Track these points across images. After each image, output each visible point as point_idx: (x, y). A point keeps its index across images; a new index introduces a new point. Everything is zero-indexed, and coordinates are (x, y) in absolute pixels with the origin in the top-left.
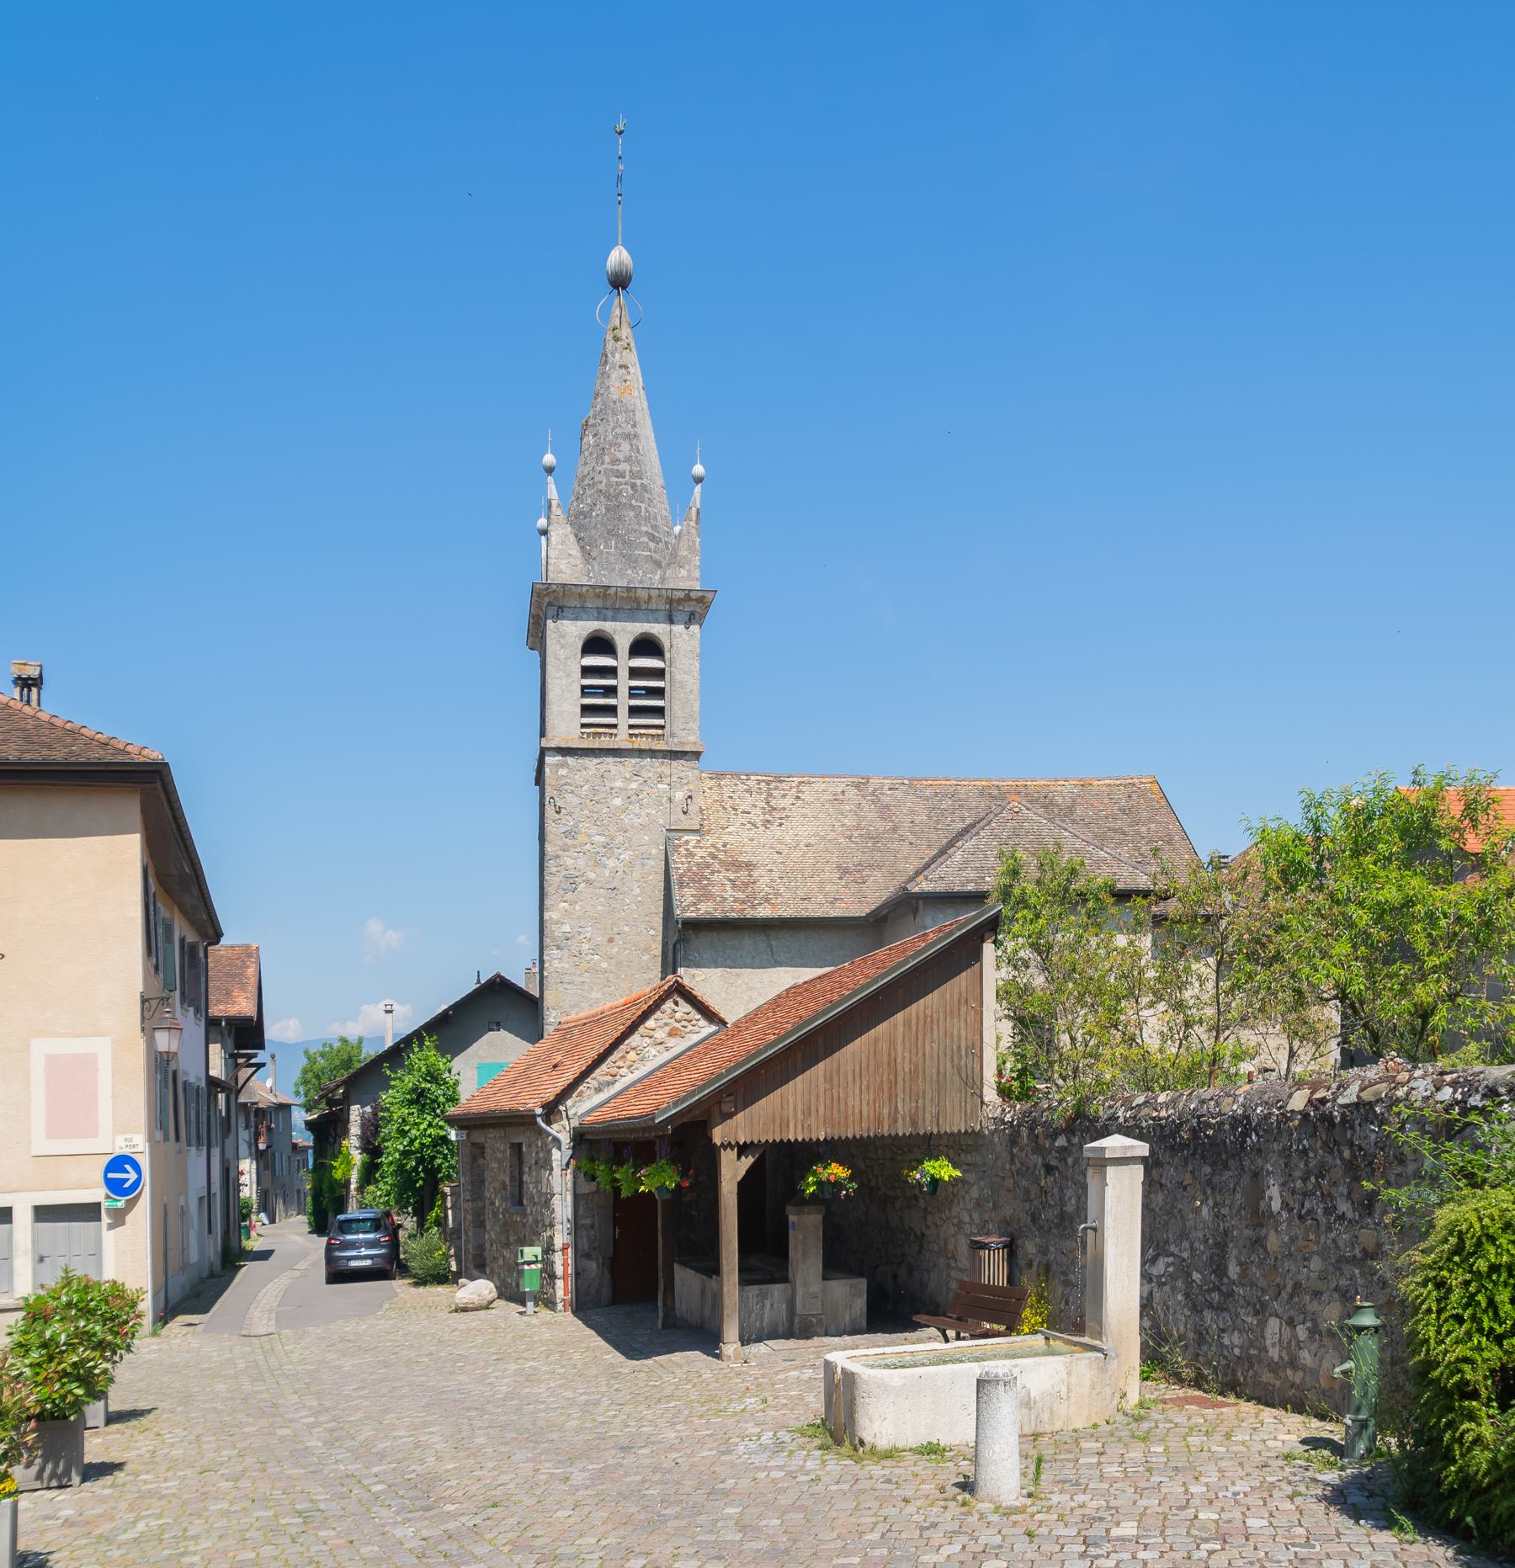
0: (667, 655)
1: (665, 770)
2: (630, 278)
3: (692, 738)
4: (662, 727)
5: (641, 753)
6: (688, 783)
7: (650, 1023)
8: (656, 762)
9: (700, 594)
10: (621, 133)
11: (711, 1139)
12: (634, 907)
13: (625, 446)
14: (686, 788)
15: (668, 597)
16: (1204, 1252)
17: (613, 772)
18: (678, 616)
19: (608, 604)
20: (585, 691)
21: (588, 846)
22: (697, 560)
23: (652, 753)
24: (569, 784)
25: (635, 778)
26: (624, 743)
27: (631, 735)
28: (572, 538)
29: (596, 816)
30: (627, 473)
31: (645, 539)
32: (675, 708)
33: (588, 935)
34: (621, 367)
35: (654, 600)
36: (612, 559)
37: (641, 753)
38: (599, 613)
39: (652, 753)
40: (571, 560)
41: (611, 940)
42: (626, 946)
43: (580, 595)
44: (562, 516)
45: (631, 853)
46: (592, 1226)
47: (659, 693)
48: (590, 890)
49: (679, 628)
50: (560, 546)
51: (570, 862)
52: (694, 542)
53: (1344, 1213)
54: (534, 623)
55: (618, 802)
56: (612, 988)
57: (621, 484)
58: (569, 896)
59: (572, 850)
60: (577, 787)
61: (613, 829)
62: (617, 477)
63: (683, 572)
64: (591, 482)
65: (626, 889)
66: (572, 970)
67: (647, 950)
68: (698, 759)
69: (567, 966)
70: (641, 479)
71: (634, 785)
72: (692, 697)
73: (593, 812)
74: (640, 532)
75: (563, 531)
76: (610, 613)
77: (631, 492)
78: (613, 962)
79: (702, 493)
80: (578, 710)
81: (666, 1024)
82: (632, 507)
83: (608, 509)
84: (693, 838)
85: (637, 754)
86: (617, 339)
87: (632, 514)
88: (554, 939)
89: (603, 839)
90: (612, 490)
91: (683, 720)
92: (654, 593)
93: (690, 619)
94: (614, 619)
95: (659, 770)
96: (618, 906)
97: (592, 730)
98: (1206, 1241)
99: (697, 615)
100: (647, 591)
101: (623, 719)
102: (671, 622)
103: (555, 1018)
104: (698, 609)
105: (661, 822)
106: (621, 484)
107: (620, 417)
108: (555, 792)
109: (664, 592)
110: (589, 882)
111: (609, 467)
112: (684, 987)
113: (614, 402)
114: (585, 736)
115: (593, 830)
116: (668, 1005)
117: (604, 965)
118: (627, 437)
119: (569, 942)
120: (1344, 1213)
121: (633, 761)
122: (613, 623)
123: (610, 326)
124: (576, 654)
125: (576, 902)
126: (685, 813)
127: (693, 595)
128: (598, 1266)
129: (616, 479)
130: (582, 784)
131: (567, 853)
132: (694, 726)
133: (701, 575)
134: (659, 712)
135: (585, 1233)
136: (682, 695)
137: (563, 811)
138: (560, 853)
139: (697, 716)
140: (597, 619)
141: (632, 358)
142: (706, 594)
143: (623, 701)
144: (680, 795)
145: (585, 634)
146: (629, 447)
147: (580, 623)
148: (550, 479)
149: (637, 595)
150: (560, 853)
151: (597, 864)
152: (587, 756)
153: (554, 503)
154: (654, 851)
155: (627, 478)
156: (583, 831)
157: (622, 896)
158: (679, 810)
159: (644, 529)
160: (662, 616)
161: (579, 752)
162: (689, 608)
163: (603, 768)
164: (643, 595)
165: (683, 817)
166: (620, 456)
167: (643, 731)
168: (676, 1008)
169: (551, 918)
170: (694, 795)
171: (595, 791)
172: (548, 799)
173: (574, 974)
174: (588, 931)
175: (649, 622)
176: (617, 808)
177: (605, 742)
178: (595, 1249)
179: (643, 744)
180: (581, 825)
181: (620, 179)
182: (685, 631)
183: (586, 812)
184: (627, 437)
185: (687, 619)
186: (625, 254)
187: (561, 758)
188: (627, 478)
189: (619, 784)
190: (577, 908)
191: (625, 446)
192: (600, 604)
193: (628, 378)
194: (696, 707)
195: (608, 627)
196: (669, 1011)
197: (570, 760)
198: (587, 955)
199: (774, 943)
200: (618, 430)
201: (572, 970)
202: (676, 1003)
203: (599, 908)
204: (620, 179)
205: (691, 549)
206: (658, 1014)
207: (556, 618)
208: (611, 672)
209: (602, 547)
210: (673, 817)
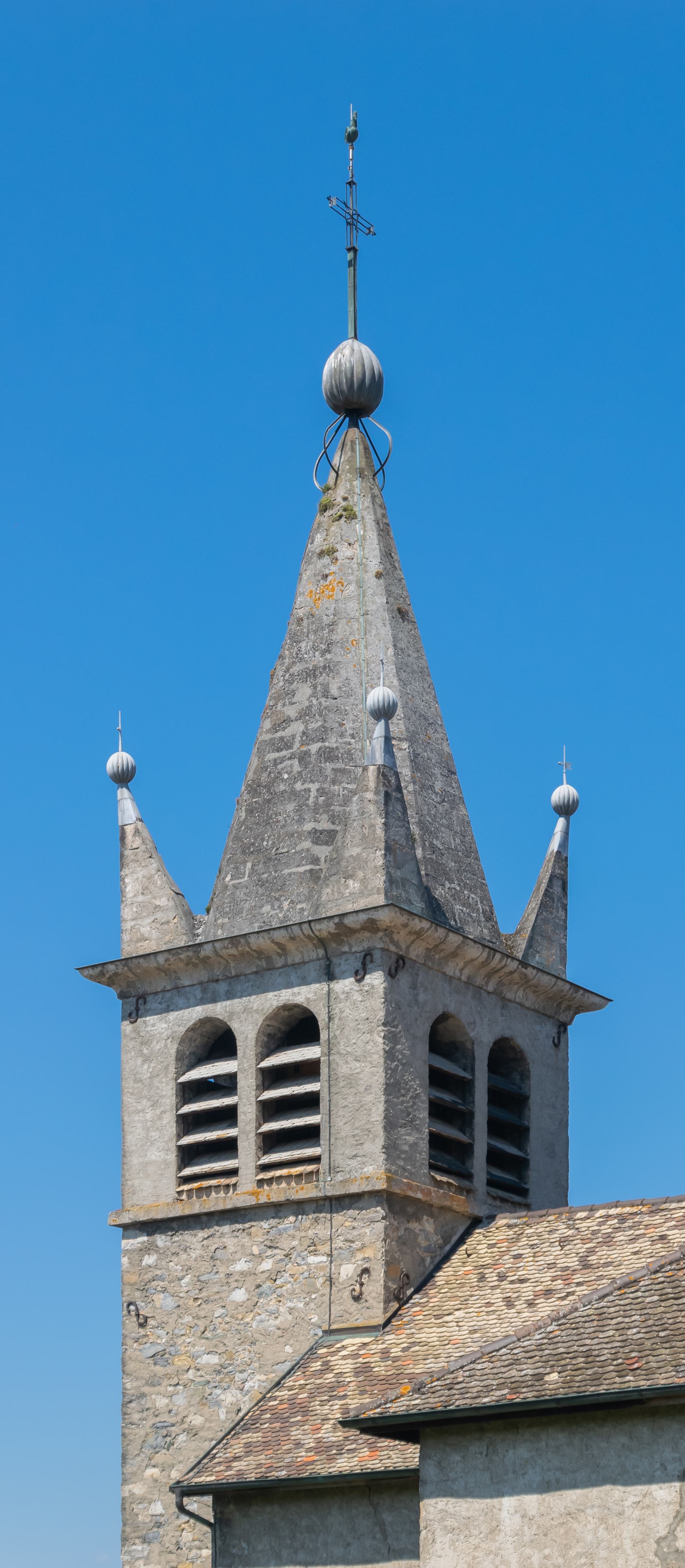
0: (323, 1036)
3: (369, 1170)
4: (316, 1160)
5: (277, 1209)
8: (306, 1220)
10: (352, 138)
14: (360, 1256)
17: (231, 1249)
18: (341, 964)
19: (218, 972)
21: (191, 1374)
23: (298, 1207)
27: (261, 1183)
29: (202, 1324)
31: (307, 844)
32: (338, 1123)
36: (240, 894)
37: (277, 1209)
38: (204, 991)
39: (298, 1207)
40: (159, 915)
47: (311, 1102)
48: (193, 1445)
49: (345, 985)
50: (140, 898)
51: (161, 1402)
55: (239, 1295)
58: (161, 1457)
59: (166, 1382)
61: (231, 1341)
63: (354, 885)
73: (198, 1317)
74: (300, 835)
76: (222, 987)
77: (297, 767)
89: (214, 1360)
90: (264, 777)
92: (280, 936)
93: (364, 964)
94: (230, 995)
97: (195, 1185)
102: (330, 976)
105: (315, 1318)
124: (167, 1068)
126: (357, 1299)
129: (276, 755)
134: (311, 1134)
137: (151, 1322)
138: (146, 1389)
140: (202, 1002)
144: (347, 1271)
147: (172, 1016)
148: (123, 794)
150: (146, 1389)
151: (204, 1401)
153: (129, 830)
158: (347, 1294)
159: (308, 826)
160: (312, 970)
162: (359, 944)
163: (214, 1243)
164: (262, 943)
165: (353, 1307)
166: (291, 712)
171: (201, 1284)
177: (216, 1202)
179: (276, 1193)
182: (356, 986)
183: (188, 1319)
184: (311, 674)
185: (358, 965)
189: (241, 1266)
191: (303, 692)
195: (219, 1010)
197: (161, 1240)
199: (387, 1517)
209: (228, 878)
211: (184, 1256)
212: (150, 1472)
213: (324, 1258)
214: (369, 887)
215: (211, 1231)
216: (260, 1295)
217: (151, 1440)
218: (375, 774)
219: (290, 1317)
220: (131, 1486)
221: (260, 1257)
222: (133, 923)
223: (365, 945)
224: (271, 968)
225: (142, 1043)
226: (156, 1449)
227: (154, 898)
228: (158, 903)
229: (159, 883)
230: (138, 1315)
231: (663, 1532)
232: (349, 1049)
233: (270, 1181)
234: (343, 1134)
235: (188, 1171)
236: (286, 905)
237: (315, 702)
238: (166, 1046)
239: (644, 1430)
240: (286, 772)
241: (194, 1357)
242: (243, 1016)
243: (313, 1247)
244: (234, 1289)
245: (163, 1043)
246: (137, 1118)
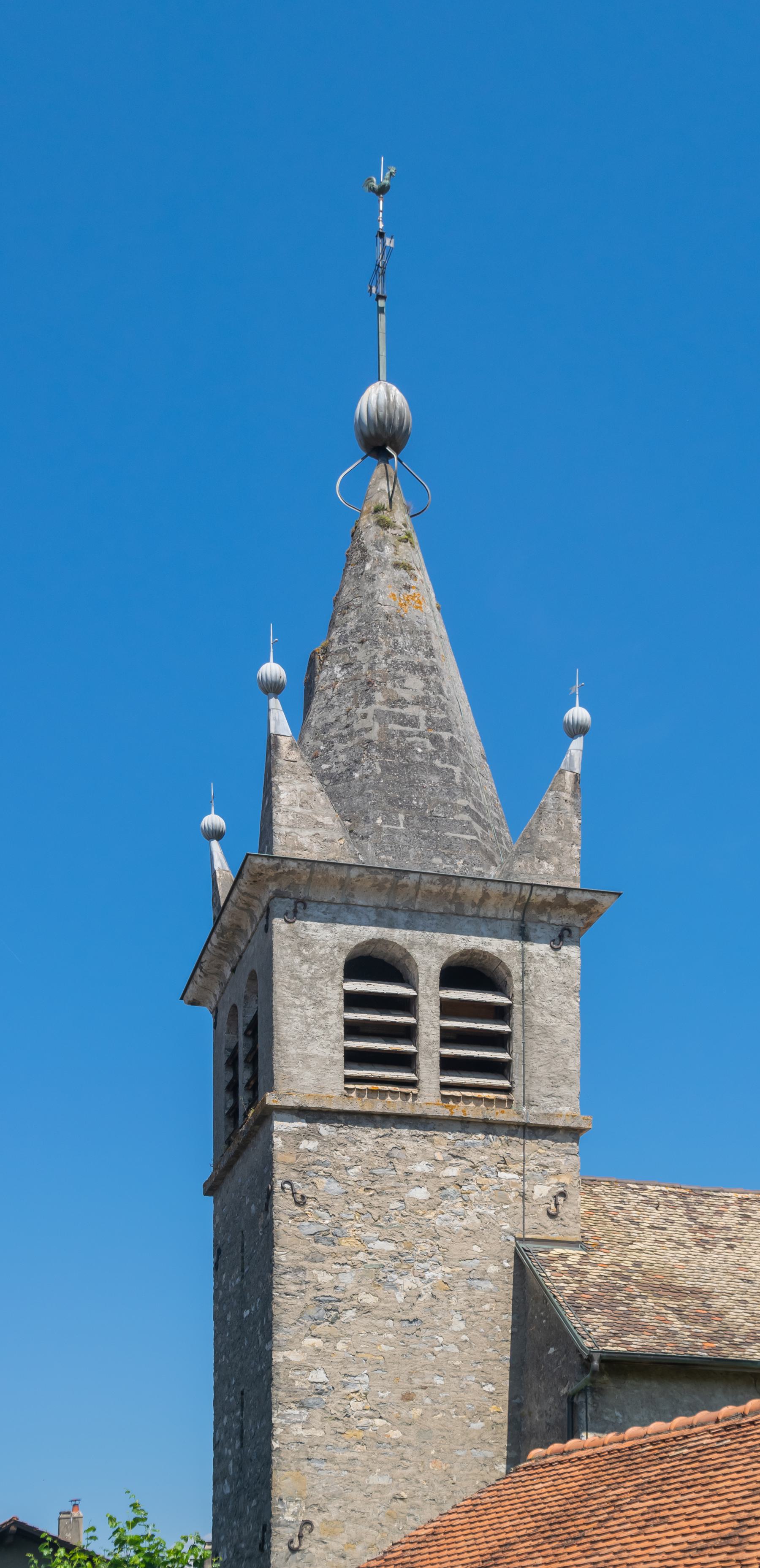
0: (517, 987)
1: (515, 1152)
2: (406, 435)
3: (565, 1109)
4: (507, 1091)
5: (465, 1124)
6: (559, 1173)
8: (496, 1141)
9: (588, 896)
12: (453, 1348)
13: (415, 683)
14: (554, 1180)
15: (520, 898)
17: (410, 1151)
19: (399, 902)
20: (501, 1041)
21: (362, 1256)
22: (575, 851)
24: (322, 1164)
25: (454, 1161)
26: (433, 1108)
28: (322, 799)
29: (375, 1213)
30: (422, 721)
33: (363, 1388)
34: (396, 565)
35: (491, 902)
38: (379, 915)
39: (489, 1127)
40: (321, 831)
41: (407, 1397)
42: (437, 1406)
43: (343, 884)
44: (302, 763)
45: (448, 1270)
47: (501, 1041)
48: (365, 1321)
50: (298, 809)
51: (324, 1278)
52: (568, 823)
54: (220, 946)
55: (421, 1194)
56: (412, 1470)
57: (410, 735)
58: (323, 1328)
59: (330, 1260)
60: (338, 1168)
62: (401, 724)
64: (345, 732)
65: (438, 1322)
66: (331, 1440)
67: (480, 1414)
68: (576, 1140)
69: (320, 1433)
70: (450, 730)
72: (566, 1050)
75: (304, 786)
76: (402, 917)
77: (430, 747)
78: (413, 1429)
79: (586, 752)
80: (340, 1056)
82: (433, 769)
83: (386, 768)
85: (459, 1126)
86: (385, 525)
87: (435, 779)
88: (292, 1392)
89: (391, 1247)
91: (549, 1082)
93: (561, 937)
95: (502, 1152)
96: (422, 1346)
99: (575, 932)
100: (482, 884)
102: (524, 935)
103: (294, 1514)
104: (578, 922)
105: (507, 1227)
106: (410, 735)
107: (400, 640)
108: (294, 1174)
109: (516, 889)
110: (363, 1310)
111: (385, 708)
113: (388, 617)
114: (354, 1094)
115: (371, 1233)
117: (396, 1434)
118: (418, 669)
119: (324, 1398)
121: (450, 1136)
122: (408, 932)
123: (370, 506)
124: (333, 974)
125: (338, 1338)
126: (552, 1216)
127: (572, 897)
130: (349, 1164)
131: (318, 1265)
132: (572, 1092)
133: (581, 873)
136: (546, 1046)
137: (311, 1203)
138: (305, 1264)
139: (577, 1078)
140: (376, 923)
141: (414, 556)
142: (599, 898)
144: (541, 1191)
145: (352, 943)
146: (422, 684)
147: (340, 928)
148: (275, 703)
149: (460, 891)
152: (358, 1123)
153: (285, 743)
154: (492, 1269)
156: (353, 1234)
157: (429, 1332)
158: (541, 1210)
161: (342, 1118)
162: (559, 918)
165: (549, 1222)
169: (286, 1360)
170: (569, 1191)
172: (279, 1183)
173: (335, 1447)
174: (363, 1382)
175: (482, 935)
176: (417, 1202)
177: (396, 1105)
180: (346, 1225)
181: (380, 271)
182: (552, 953)
185: (555, 935)
186: (397, 395)
187: (305, 1125)
188: (423, 727)
189: (421, 1167)
190: (340, 1346)
192: (382, 900)
193: (413, 583)
194: (575, 1064)
197: (324, 1129)
198: (360, 1418)
201: (331, 1440)
203: (384, 1348)
204: (380, 271)
205: (563, 832)
207: (292, 915)
209: (379, 821)
210: (530, 1222)
212: (309, 1342)
213: (516, 1176)
214: (565, 873)
215: (387, 1131)
216: (445, 1197)
217: (313, 1312)
218: (573, 779)
219: (478, 1221)
220: (285, 1353)
221: (443, 1163)
222: (288, 830)
223: (565, 921)
224: (460, 913)
225: (300, 944)
226: (317, 1321)
227: (316, 814)
228: (320, 819)
229: (322, 801)
230: (294, 1194)
232: (544, 1004)
233: (456, 1099)
234: (538, 1074)
235: (447, 1079)
236: (460, 863)
237: (431, 694)
238: (332, 953)
240: (420, 747)
242: (426, 949)
244: (413, 1187)
245: (328, 950)
246: (294, 1011)
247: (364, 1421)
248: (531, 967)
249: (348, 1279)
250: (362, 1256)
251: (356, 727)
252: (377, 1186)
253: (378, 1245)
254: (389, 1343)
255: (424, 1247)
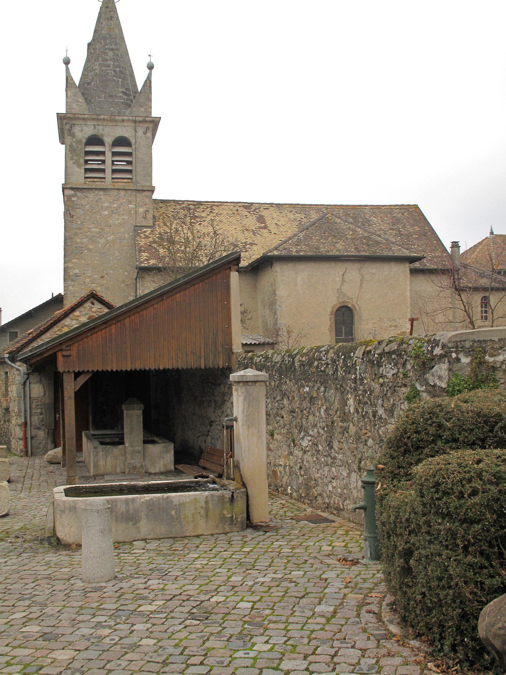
0: (134, 146)
4: (131, 179)
7: (77, 313)
11: (56, 368)
13: (111, 54)
16: (323, 435)
17: (103, 200)
21: (89, 233)
28: (80, 94)
30: (112, 66)
31: (121, 95)
33: (90, 275)
40: (79, 103)
41: (102, 277)
46: (41, 414)
51: (78, 240)
53: (381, 415)
55: (106, 213)
71: (115, 205)
77: (113, 73)
81: (86, 314)
84: (149, 230)
89: (97, 230)
95: (129, 199)
98: (324, 429)
101: (108, 174)
106: (108, 70)
110: (89, 250)
111: (101, 63)
112: (97, 295)
116: (88, 305)
118: (112, 50)
120: (381, 415)
128: (45, 434)
135: (36, 418)
137: (75, 217)
138: (73, 236)
143: (108, 167)
144: (141, 210)
154: (127, 236)
155: (112, 68)
158: (141, 216)
159: (121, 90)
165: (143, 220)
166: (108, 58)
167: (120, 180)
168: (93, 306)
177: (99, 185)
178: (43, 425)
179: (120, 185)
180: (85, 223)
188: (112, 68)
189: (106, 204)
196: (89, 308)
197: (79, 194)
198: (88, 284)
200: (106, 47)
202: (93, 304)
206: (81, 309)
208: (103, 153)
211: (87, 199)
212: (74, 260)
216: (113, 213)
221: (113, 203)
231: (338, 287)
235: (114, 177)
239: (333, 264)
241: (90, 228)
243: (130, 202)
247: (90, 285)
248: (138, 140)
249: (85, 240)
250: (89, 233)
251: (94, 68)
252: (94, 211)
253: (94, 229)
254: (97, 260)
255: (107, 229)
